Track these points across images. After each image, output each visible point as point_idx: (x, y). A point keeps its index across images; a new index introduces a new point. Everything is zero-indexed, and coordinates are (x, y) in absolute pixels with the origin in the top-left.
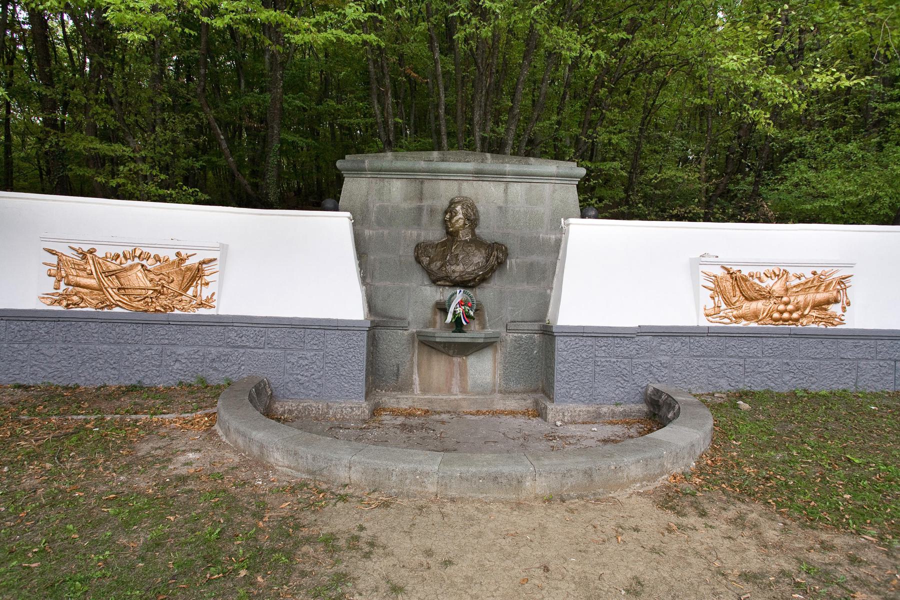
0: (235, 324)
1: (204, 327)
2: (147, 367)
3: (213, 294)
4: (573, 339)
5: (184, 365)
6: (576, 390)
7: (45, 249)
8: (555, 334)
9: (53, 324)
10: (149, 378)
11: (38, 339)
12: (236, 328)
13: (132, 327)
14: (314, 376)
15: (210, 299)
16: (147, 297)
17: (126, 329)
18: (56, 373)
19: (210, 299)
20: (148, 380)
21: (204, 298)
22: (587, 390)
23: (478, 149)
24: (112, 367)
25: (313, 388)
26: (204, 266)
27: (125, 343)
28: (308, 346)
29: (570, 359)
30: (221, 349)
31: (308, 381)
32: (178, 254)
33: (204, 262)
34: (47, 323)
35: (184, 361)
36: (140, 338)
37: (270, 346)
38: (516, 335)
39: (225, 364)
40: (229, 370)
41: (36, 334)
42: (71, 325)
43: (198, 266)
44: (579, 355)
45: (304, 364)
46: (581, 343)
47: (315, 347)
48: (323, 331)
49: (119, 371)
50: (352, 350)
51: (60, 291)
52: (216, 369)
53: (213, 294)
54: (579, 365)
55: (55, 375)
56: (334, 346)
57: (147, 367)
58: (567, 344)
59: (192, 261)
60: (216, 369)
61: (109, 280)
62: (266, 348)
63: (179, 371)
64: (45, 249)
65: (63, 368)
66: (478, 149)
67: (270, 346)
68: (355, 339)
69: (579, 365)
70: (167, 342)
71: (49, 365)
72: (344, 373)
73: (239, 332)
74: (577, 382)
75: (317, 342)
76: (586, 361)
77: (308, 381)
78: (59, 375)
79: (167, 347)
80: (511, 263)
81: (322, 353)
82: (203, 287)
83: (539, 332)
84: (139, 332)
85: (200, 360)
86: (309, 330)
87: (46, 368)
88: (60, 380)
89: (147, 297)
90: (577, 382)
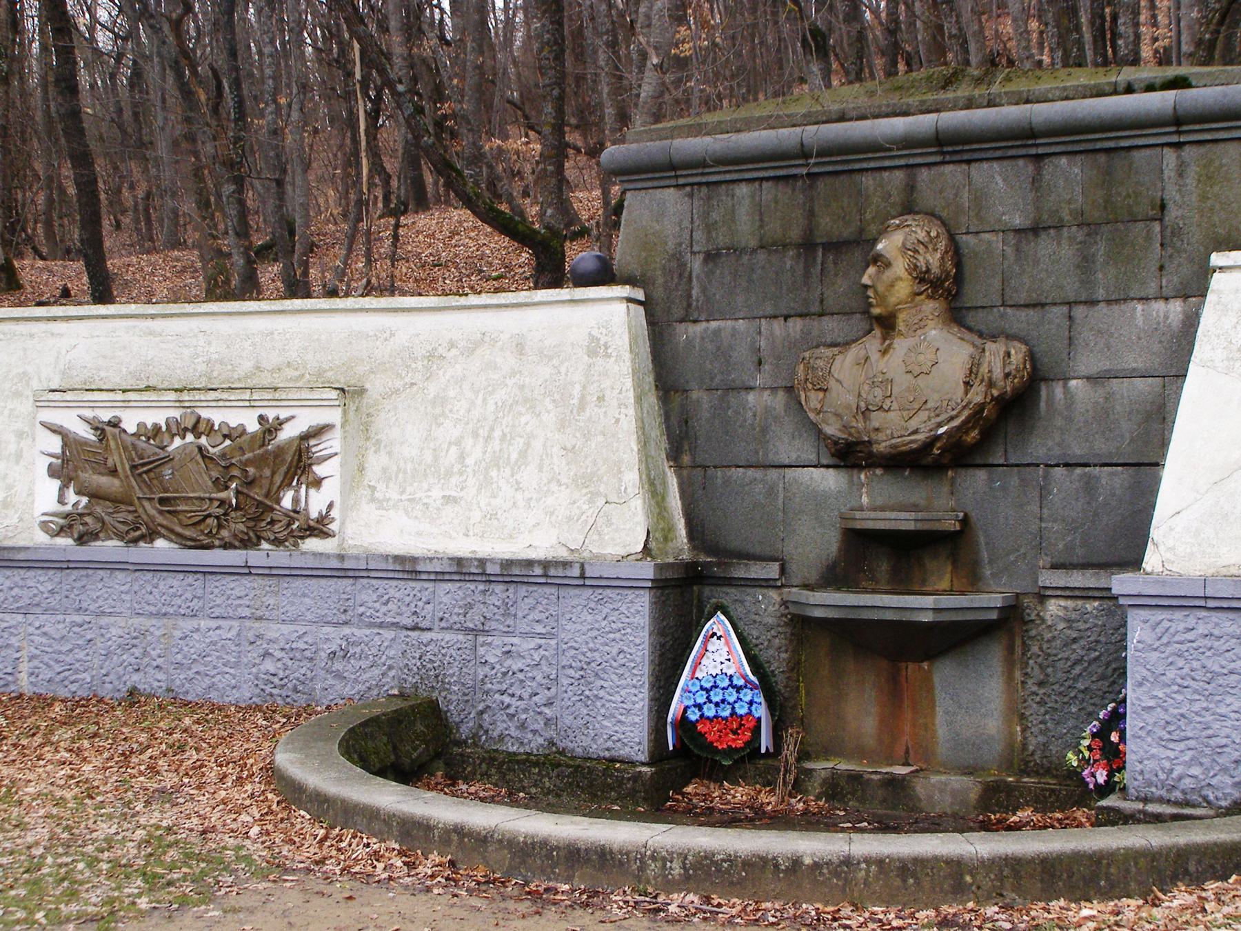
0: (373, 574)
1: (314, 581)
2: (215, 667)
3: (330, 506)
4: (1178, 615)
5: (279, 665)
6: (1189, 764)
7: (43, 424)
8: (1122, 601)
9: (59, 574)
10: (217, 690)
11: (38, 605)
12: (374, 582)
13: (185, 583)
14: (536, 699)
15: (323, 519)
16: (209, 516)
17: (175, 583)
18: (67, 673)
19: (323, 519)
20: (216, 693)
21: (314, 514)
22: (1224, 770)
23: (1174, 63)
24: (155, 664)
25: (536, 726)
26: (312, 442)
27: (176, 614)
28: (523, 626)
29: (1171, 674)
30: (346, 630)
31: (526, 710)
32: (262, 419)
33: (305, 437)
34: (51, 572)
35: (278, 654)
36: (200, 604)
37: (443, 624)
38: (1070, 603)
39: (358, 664)
40: (365, 677)
41: (35, 595)
42: (87, 576)
43: (299, 446)
44: (1195, 664)
45: (515, 668)
46: (1202, 629)
47: (539, 629)
48: (554, 590)
49: (166, 673)
50: (618, 635)
51: (68, 508)
52: (339, 676)
53: (330, 506)
54: (1195, 691)
55: (66, 678)
56: (578, 627)
57: (215, 667)
58: (1159, 630)
59: (288, 433)
60: (339, 676)
61: (144, 481)
62: (436, 628)
63: (271, 678)
64: (43, 424)
65: (77, 665)
66: (1174, 63)
67: (443, 624)
68: (623, 609)
69: (1195, 691)
70: (247, 612)
71: (56, 656)
72: (602, 693)
73: (381, 591)
74: (1192, 743)
75: (543, 616)
76: (1221, 681)
77: (526, 710)
78: (72, 678)
79: (247, 623)
80: (1050, 399)
81: (553, 642)
82: (312, 491)
83: (649, 584)
84: (199, 592)
85: (308, 654)
86: (524, 588)
87: (52, 663)
88: (73, 688)
89: (209, 516)
90: (1192, 743)
